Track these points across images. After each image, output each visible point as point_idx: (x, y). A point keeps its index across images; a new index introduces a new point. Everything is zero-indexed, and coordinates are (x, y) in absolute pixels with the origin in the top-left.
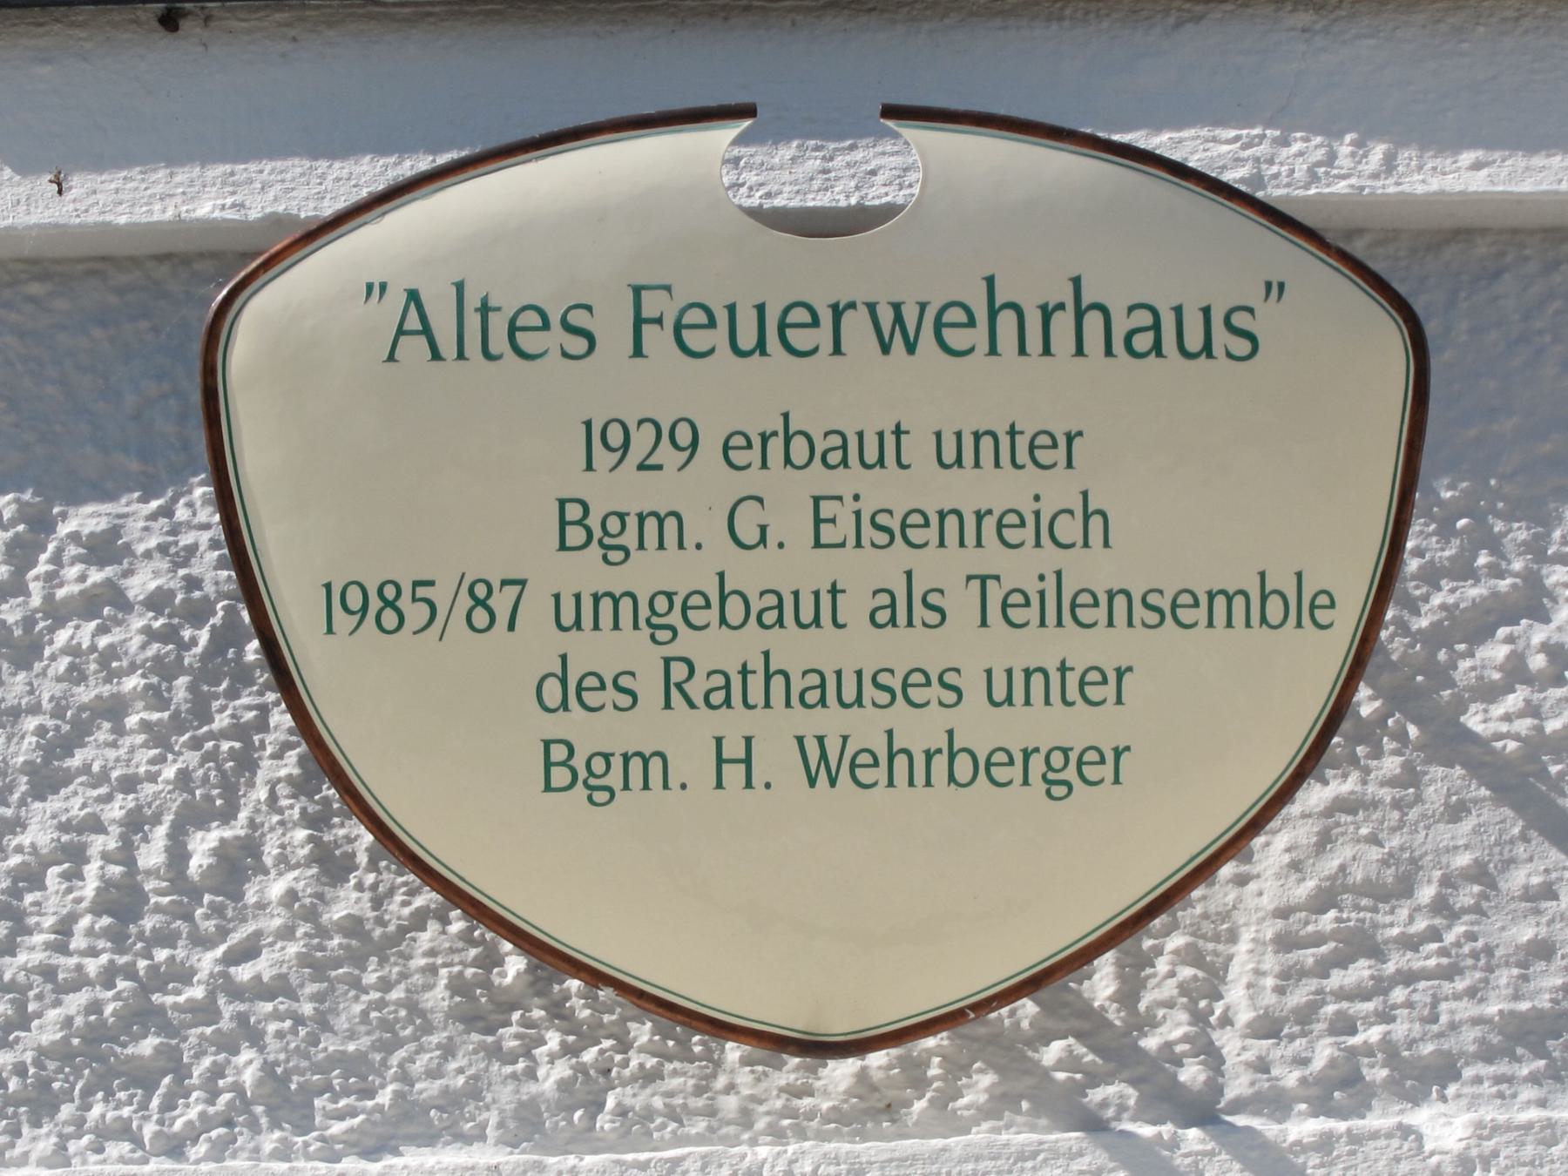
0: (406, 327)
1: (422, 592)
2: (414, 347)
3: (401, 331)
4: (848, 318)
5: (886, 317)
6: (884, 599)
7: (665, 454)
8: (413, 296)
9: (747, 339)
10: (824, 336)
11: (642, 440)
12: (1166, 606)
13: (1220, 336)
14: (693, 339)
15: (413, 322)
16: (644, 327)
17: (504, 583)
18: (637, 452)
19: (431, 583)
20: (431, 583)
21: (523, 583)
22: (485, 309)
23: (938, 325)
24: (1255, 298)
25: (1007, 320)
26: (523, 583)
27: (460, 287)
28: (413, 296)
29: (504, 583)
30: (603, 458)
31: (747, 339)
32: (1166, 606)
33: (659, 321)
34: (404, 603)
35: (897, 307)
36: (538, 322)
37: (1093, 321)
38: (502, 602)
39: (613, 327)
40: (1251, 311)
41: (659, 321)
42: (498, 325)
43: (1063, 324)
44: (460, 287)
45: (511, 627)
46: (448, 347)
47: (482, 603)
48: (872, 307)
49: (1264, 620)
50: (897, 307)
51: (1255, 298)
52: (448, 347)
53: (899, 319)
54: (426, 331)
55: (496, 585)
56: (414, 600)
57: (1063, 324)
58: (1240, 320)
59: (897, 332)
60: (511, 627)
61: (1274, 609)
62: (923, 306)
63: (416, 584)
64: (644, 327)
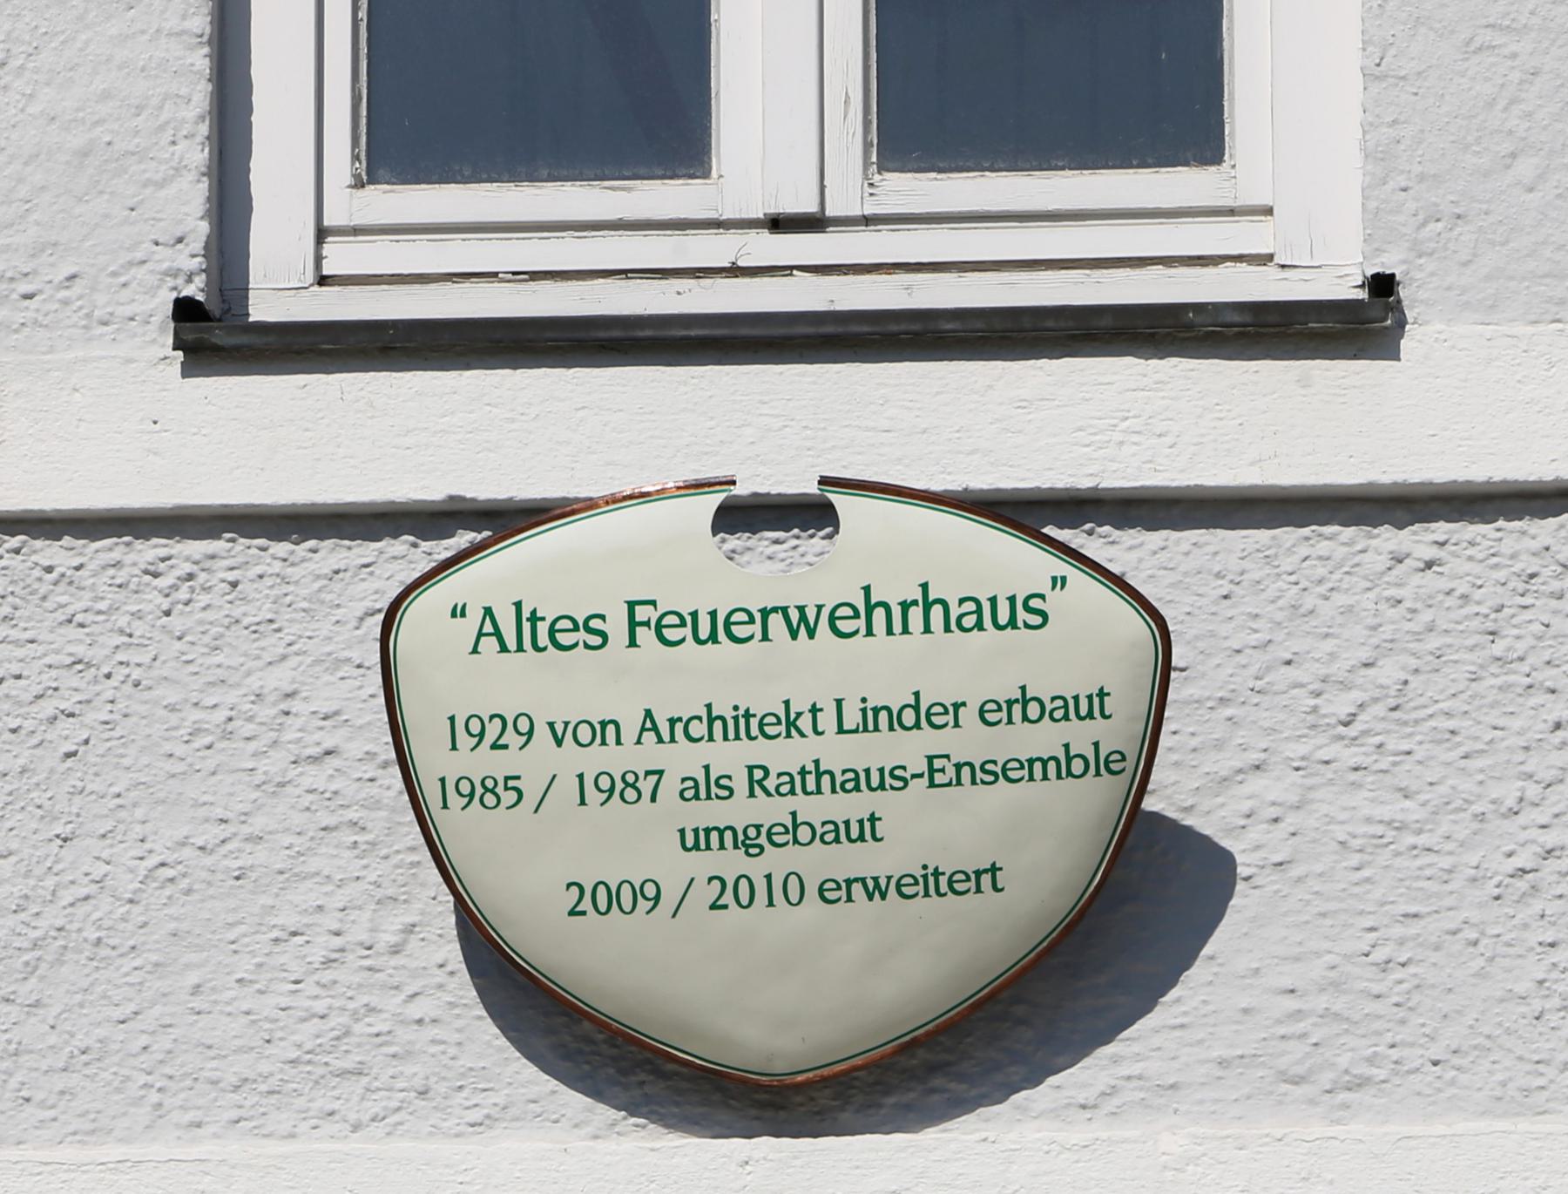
0: (485, 631)
1: (511, 783)
2: (489, 644)
3: (480, 634)
4: (773, 617)
5: (794, 616)
6: (690, 783)
7: (510, 737)
8: (488, 611)
9: (704, 633)
10: (757, 628)
11: (493, 729)
12: (998, 769)
13: (1022, 615)
14: (669, 634)
15: (488, 628)
16: (638, 629)
17: (648, 773)
18: (490, 737)
19: (518, 778)
20: (518, 778)
21: (660, 773)
22: (534, 619)
23: (832, 619)
24: (1045, 588)
25: (879, 613)
26: (660, 773)
27: (518, 605)
28: (488, 611)
29: (648, 773)
30: (464, 741)
31: (704, 633)
32: (998, 769)
33: (647, 624)
34: (500, 790)
35: (801, 609)
36: (571, 626)
37: (937, 611)
38: (646, 786)
39: (616, 626)
40: (1042, 597)
41: (647, 624)
42: (543, 628)
43: (916, 614)
44: (518, 605)
45: (653, 799)
46: (511, 643)
47: (633, 786)
48: (784, 610)
49: (1069, 773)
50: (801, 609)
51: (1045, 588)
52: (511, 643)
53: (803, 617)
54: (497, 633)
55: (641, 776)
56: (506, 788)
57: (916, 614)
58: (1034, 603)
59: (801, 624)
60: (653, 799)
61: (1077, 767)
62: (820, 607)
63: (507, 779)
64: (638, 629)
